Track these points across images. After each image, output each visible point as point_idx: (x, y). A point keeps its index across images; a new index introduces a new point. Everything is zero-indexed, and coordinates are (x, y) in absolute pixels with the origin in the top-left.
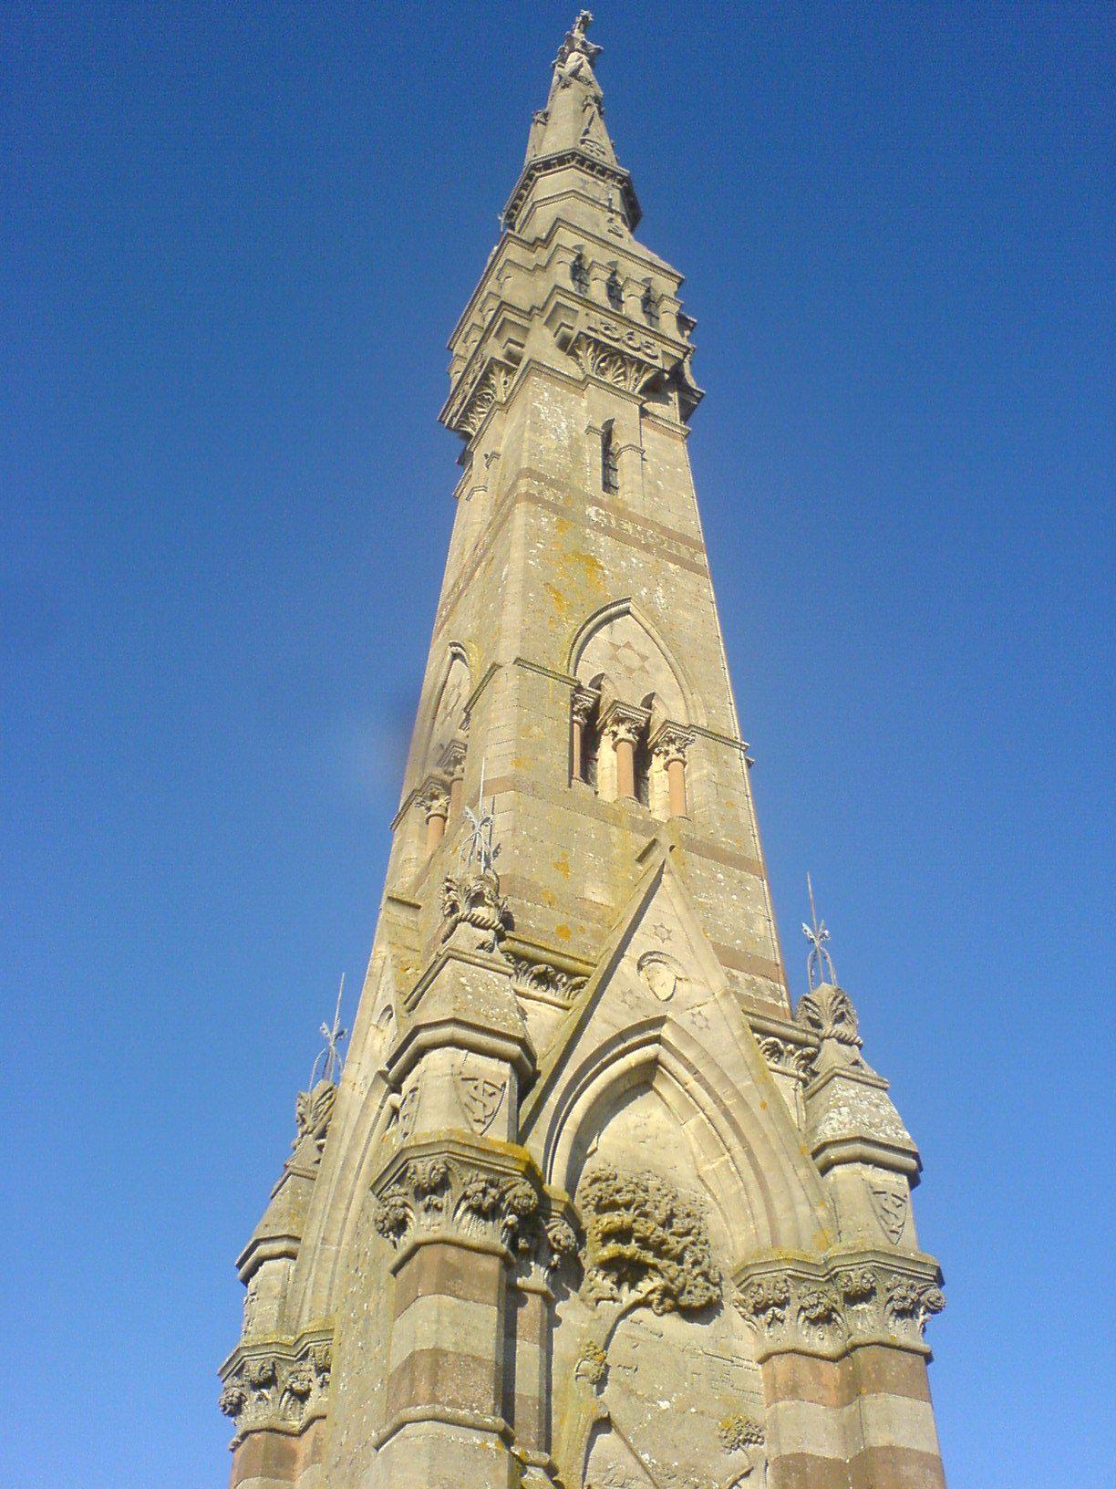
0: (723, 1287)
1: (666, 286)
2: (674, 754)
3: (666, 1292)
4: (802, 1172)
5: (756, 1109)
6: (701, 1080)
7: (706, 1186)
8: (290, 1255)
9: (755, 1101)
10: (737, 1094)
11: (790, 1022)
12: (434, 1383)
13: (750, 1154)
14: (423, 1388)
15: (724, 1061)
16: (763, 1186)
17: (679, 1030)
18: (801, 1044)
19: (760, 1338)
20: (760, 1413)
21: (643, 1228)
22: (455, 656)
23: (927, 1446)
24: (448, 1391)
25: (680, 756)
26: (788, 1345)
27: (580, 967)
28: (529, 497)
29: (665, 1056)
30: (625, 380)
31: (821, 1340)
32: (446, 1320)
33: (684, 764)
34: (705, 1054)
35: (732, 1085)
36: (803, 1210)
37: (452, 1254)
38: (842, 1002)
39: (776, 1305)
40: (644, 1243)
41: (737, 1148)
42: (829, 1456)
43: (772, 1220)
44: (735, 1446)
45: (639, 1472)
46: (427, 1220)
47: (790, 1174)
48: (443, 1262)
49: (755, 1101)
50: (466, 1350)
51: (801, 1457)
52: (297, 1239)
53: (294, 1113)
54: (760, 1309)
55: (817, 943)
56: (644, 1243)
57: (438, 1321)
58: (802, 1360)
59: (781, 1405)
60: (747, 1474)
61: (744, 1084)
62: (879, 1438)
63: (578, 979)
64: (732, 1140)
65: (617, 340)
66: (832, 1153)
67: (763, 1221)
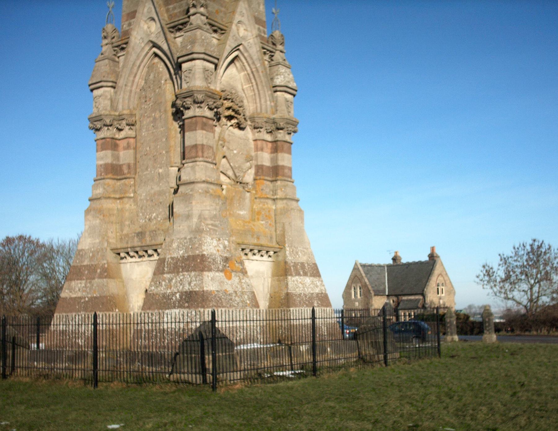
0: (183, 77)
3: (238, 123)
4: (270, 92)
6: (247, 62)
8: (114, 87)
9: (260, 70)
10: (256, 68)
11: (266, 44)
13: (257, 84)
17: (245, 48)
18: (271, 52)
19: (254, 134)
20: (253, 154)
24: (205, 154)
26: (262, 138)
27: (225, 28)
31: (269, 138)
36: (268, 103)
37: (204, 120)
40: (234, 110)
41: (254, 84)
43: (261, 105)
45: (230, 167)
46: (197, 110)
47: (266, 92)
48: (203, 122)
49: (260, 70)
54: (255, 128)
57: (202, 137)
58: (264, 142)
62: (281, 163)
63: (223, 32)
64: (253, 81)
66: (278, 89)
67: (259, 105)
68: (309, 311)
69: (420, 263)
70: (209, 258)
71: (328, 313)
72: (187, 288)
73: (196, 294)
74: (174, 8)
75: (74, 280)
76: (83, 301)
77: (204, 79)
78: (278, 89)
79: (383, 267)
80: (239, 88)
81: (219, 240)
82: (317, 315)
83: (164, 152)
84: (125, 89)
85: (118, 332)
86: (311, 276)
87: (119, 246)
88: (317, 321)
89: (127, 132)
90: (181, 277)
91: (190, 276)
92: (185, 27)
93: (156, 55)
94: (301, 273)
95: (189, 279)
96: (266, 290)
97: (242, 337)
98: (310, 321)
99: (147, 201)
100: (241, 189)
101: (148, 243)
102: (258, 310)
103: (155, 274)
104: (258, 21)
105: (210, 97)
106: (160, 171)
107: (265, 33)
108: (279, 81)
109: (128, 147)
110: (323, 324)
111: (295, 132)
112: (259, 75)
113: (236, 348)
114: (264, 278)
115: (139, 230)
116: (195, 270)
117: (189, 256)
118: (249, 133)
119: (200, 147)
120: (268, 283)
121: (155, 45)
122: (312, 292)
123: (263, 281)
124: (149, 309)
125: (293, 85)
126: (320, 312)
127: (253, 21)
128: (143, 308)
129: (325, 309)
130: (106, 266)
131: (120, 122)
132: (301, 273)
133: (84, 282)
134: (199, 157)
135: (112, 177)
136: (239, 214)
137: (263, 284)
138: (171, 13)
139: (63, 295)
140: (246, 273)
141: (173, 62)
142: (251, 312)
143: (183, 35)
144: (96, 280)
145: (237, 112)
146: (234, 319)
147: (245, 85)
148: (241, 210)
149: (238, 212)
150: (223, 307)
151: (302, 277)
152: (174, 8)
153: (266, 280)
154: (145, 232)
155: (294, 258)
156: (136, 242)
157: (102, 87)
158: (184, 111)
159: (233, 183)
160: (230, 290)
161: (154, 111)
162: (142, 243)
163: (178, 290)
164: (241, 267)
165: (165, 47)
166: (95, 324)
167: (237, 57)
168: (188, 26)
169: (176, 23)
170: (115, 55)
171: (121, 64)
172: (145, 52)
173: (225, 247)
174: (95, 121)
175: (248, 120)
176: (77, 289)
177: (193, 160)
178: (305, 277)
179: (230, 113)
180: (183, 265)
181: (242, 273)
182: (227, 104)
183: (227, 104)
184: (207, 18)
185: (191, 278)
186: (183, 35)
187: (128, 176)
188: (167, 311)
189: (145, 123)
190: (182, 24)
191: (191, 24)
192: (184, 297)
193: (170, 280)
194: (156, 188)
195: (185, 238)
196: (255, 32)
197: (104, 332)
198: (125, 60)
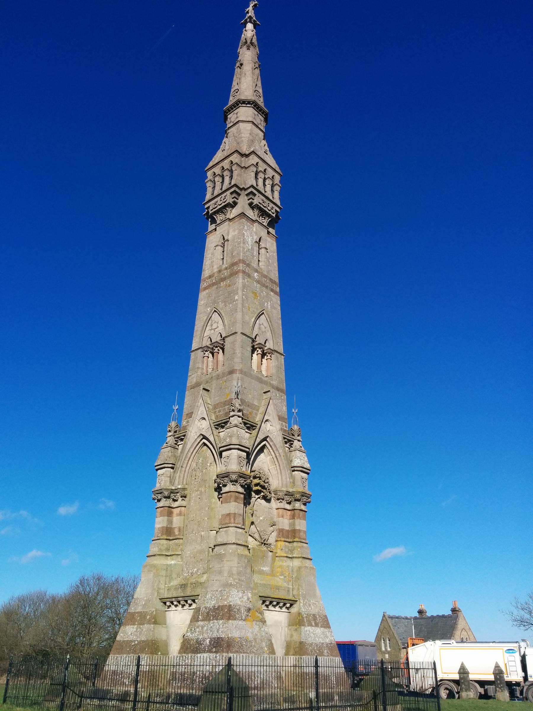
1: (277, 178)
2: (269, 357)
4: (289, 471)
5: (282, 457)
6: (272, 449)
7: (270, 471)
8: (173, 468)
9: (282, 454)
10: (279, 453)
12: (234, 519)
13: (279, 465)
14: (232, 520)
15: (278, 446)
16: (281, 473)
17: (270, 439)
18: (291, 441)
20: (275, 520)
21: (262, 483)
22: (215, 311)
23: (305, 530)
25: (270, 358)
28: (244, 272)
29: (267, 444)
30: (264, 219)
31: (288, 507)
32: (236, 507)
33: (271, 360)
34: (274, 444)
35: (279, 451)
36: (288, 479)
38: (300, 431)
39: (282, 499)
40: (261, 486)
41: (277, 465)
42: (287, 529)
44: (272, 526)
46: (232, 486)
48: (235, 495)
49: (282, 454)
50: (239, 513)
51: (283, 529)
52: (175, 465)
53: (167, 429)
54: (278, 499)
55: (295, 414)
56: (261, 486)
59: (280, 519)
60: (273, 532)
61: (281, 451)
62: (297, 528)
64: (277, 463)
65: (265, 207)
66: (296, 469)
67: (280, 481)
68: (312, 659)
69: (443, 616)
70: (234, 608)
71: (337, 662)
72: (215, 635)
73: (222, 640)
74: (220, 411)
75: (128, 625)
76: (133, 644)
77: (238, 463)
78: (296, 469)
79: (410, 619)
80: (266, 469)
81: (244, 592)
82: (320, 664)
83: (206, 519)
84: (181, 469)
85: (158, 674)
86: (321, 627)
87: (166, 596)
88: (320, 670)
89: (180, 502)
90: (212, 625)
91: (218, 624)
92: (226, 425)
93: (205, 444)
94: (313, 624)
95: (218, 626)
96: (283, 638)
97: (259, 682)
98: (313, 670)
99: (191, 558)
100: (265, 549)
101: (188, 594)
102: (273, 656)
103: (191, 621)
104: (280, 418)
105: (241, 477)
106: (202, 533)
107: (286, 428)
108: (297, 462)
109: (180, 514)
110: (332, 673)
111: (309, 502)
112: (281, 459)
113: (250, 692)
114: (282, 627)
115: (183, 582)
116: (222, 619)
117: (219, 607)
118: (274, 504)
119: (232, 516)
120: (285, 632)
121: (205, 437)
122: (322, 642)
123: (280, 630)
124: (185, 653)
125: (307, 465)
126: (330, 661)
127: (276, 418)
128: (180, 652)
129: (334, 658)
130: (154, 613)
131: (175, 495)
132: (313, 624)
133: (136, 626)
134: (232, 524)
135: (165, 537)
136: (263, 570)
137: (281, 633)
138: (217, 414)
139: (118, 638)
140: (265, 622)
141: (217, 450)
142: (268, 658)
143: (224, 431)
144: (145, 625)
145: (263, 487)
146: (253, 665)
147: (271, 466)
148: (264, 566)
149: (262, 568)
150: (244, 653)
151: (313, 628)
152: (220, 411)
153: (284, 629)
154: (187, 584)
155: (307, 610)
156: (180, 593)
157: (164, 468)
158: (222, 488)
159: (258, 543)
160: (250, 636)
161: (201, 487)
162: (184, 594)
163: (208, 636)
164: (261, 617)
165: (211, 439)
166: (138, 665)
167: (265, 445)
168: (228, 425)
169: (220, 422)
170: (176, 444)
171: (180, 450)
172: (197, 442)
173: (248, 599)
174: (157, 494)
175: (273, 493)
176: (130, 633)
177: (227, 525)
178: (316, 628)
179: (259, 488)
180: (214, 613)
181: (262, 622)
182: (256, 481)
183: (256, 481)
184: (242, 419)
185: (220, 626)
186: (224, 431)
187: (178, 537)
188: (199, 655)
189: (193, 495)
190: (224, 423)
191: (231, 423)
192: (212, 642)
193: (203, 627)
194: (198, 548)
195: (217, 591)
196: (278, 427)
197: (147, 673)
198: (183, 447)
